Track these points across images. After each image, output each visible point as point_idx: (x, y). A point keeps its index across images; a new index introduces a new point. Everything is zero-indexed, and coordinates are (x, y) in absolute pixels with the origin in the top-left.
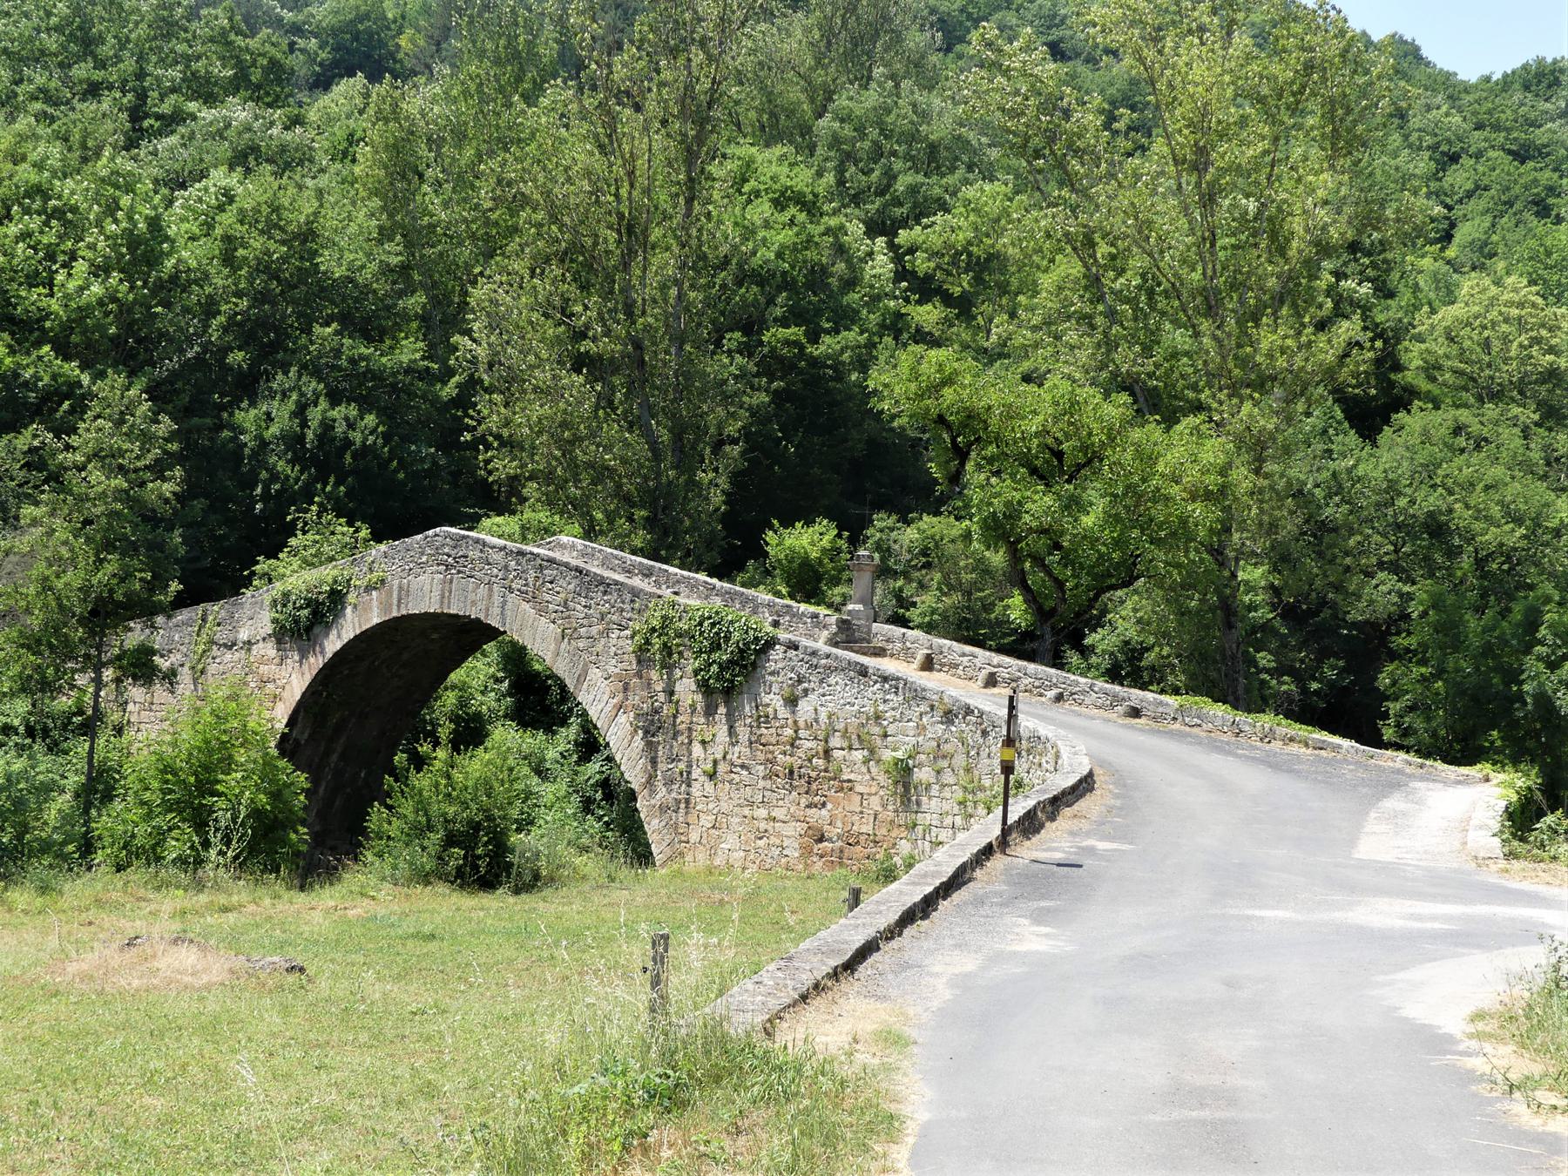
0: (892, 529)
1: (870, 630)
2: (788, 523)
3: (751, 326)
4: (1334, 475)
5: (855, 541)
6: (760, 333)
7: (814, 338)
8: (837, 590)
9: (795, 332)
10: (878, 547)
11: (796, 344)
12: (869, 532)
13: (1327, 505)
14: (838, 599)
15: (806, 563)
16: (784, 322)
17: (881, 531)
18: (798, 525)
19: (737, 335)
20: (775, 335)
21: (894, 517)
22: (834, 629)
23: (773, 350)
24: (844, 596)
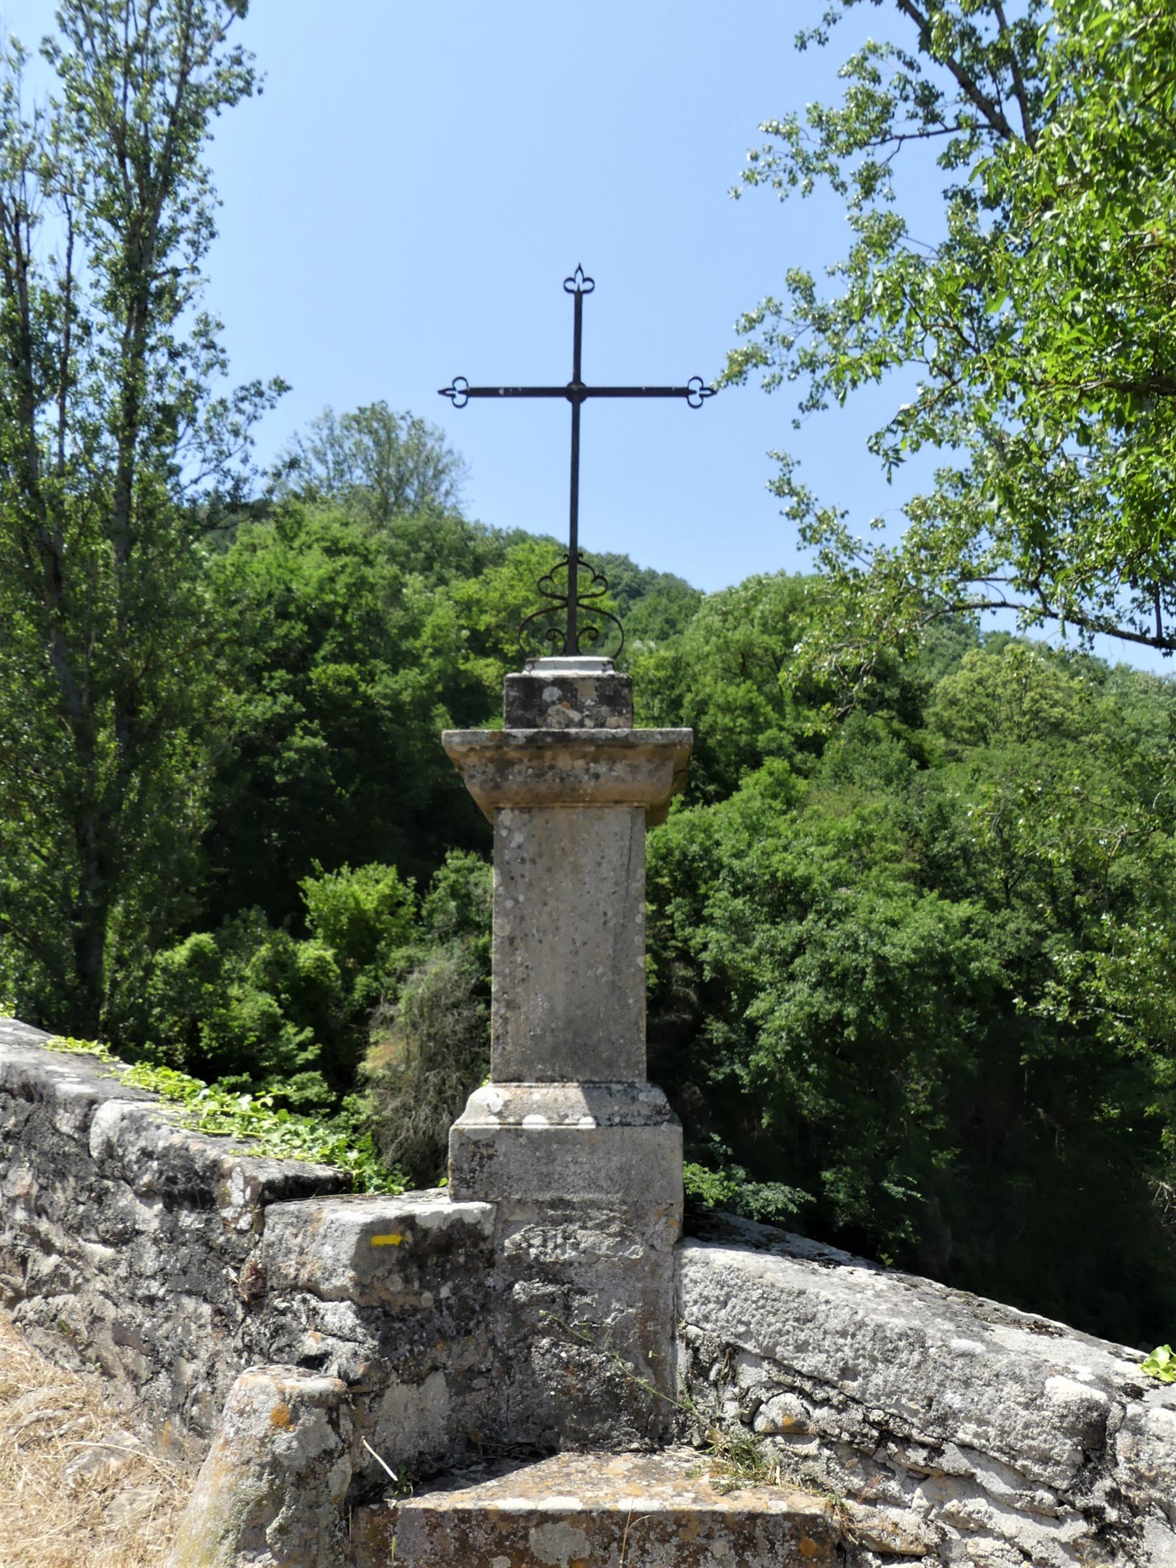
0: (471, 870)
1: (660, 1314)
2: (331, 866)
3: (297, 660)
4: (939, 806)
5: (422, 889)
6: (306, 669)
7: (371, 678)
8: (404, 951)
9: (346, 670)
10: (454, 893)
11: (349, 682)
12: (438, 874)
13: (935, 839)
14: (401, 964)
15: (359, 920)
16: (333, 658)
17: (457, 871)
18: (345, 870)
19: (281, 673)
20: (325, 673)
21: (473, 856)
22: (337, 1329)
23: (324, 689)
24: (409, 959)
